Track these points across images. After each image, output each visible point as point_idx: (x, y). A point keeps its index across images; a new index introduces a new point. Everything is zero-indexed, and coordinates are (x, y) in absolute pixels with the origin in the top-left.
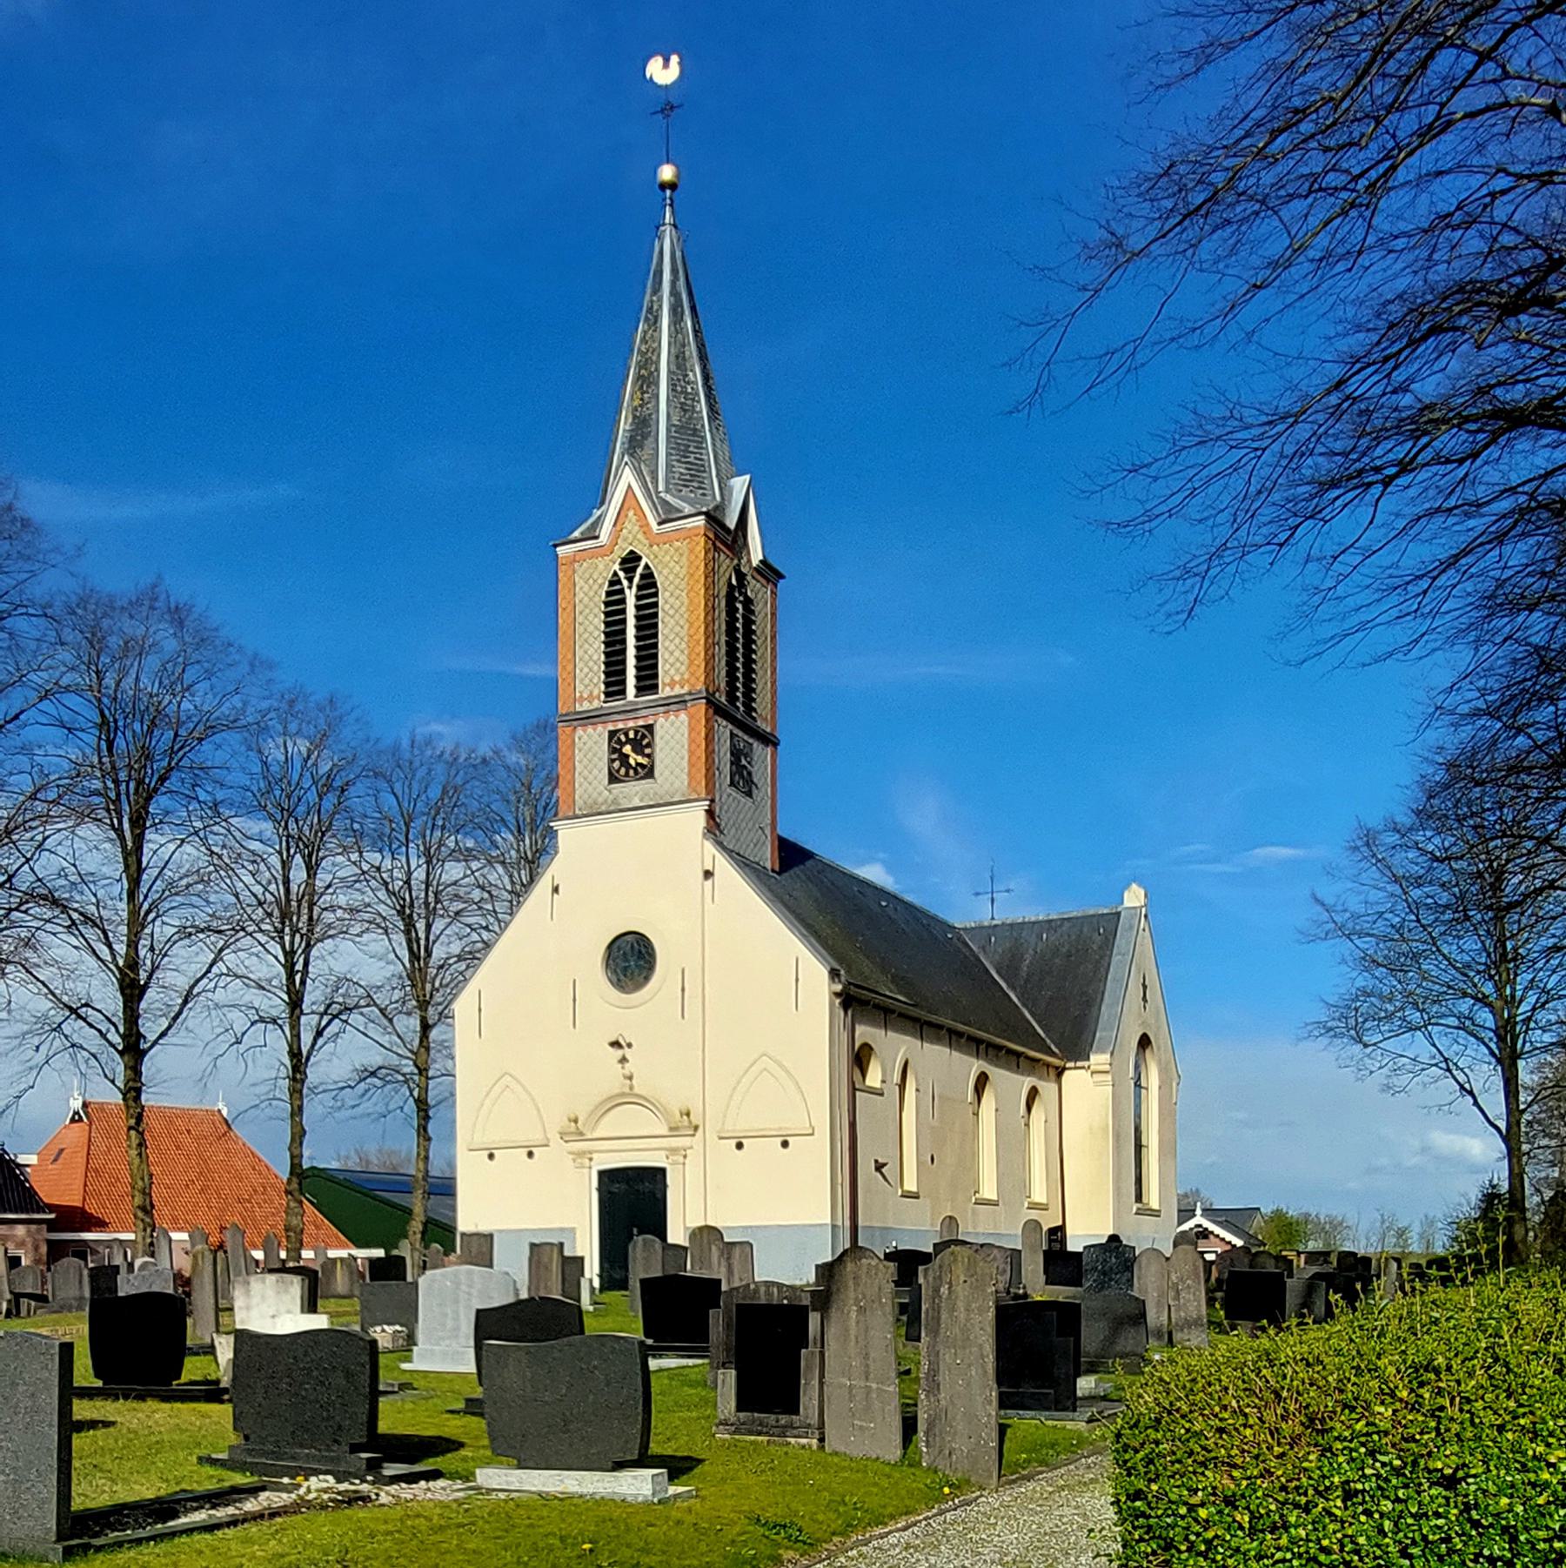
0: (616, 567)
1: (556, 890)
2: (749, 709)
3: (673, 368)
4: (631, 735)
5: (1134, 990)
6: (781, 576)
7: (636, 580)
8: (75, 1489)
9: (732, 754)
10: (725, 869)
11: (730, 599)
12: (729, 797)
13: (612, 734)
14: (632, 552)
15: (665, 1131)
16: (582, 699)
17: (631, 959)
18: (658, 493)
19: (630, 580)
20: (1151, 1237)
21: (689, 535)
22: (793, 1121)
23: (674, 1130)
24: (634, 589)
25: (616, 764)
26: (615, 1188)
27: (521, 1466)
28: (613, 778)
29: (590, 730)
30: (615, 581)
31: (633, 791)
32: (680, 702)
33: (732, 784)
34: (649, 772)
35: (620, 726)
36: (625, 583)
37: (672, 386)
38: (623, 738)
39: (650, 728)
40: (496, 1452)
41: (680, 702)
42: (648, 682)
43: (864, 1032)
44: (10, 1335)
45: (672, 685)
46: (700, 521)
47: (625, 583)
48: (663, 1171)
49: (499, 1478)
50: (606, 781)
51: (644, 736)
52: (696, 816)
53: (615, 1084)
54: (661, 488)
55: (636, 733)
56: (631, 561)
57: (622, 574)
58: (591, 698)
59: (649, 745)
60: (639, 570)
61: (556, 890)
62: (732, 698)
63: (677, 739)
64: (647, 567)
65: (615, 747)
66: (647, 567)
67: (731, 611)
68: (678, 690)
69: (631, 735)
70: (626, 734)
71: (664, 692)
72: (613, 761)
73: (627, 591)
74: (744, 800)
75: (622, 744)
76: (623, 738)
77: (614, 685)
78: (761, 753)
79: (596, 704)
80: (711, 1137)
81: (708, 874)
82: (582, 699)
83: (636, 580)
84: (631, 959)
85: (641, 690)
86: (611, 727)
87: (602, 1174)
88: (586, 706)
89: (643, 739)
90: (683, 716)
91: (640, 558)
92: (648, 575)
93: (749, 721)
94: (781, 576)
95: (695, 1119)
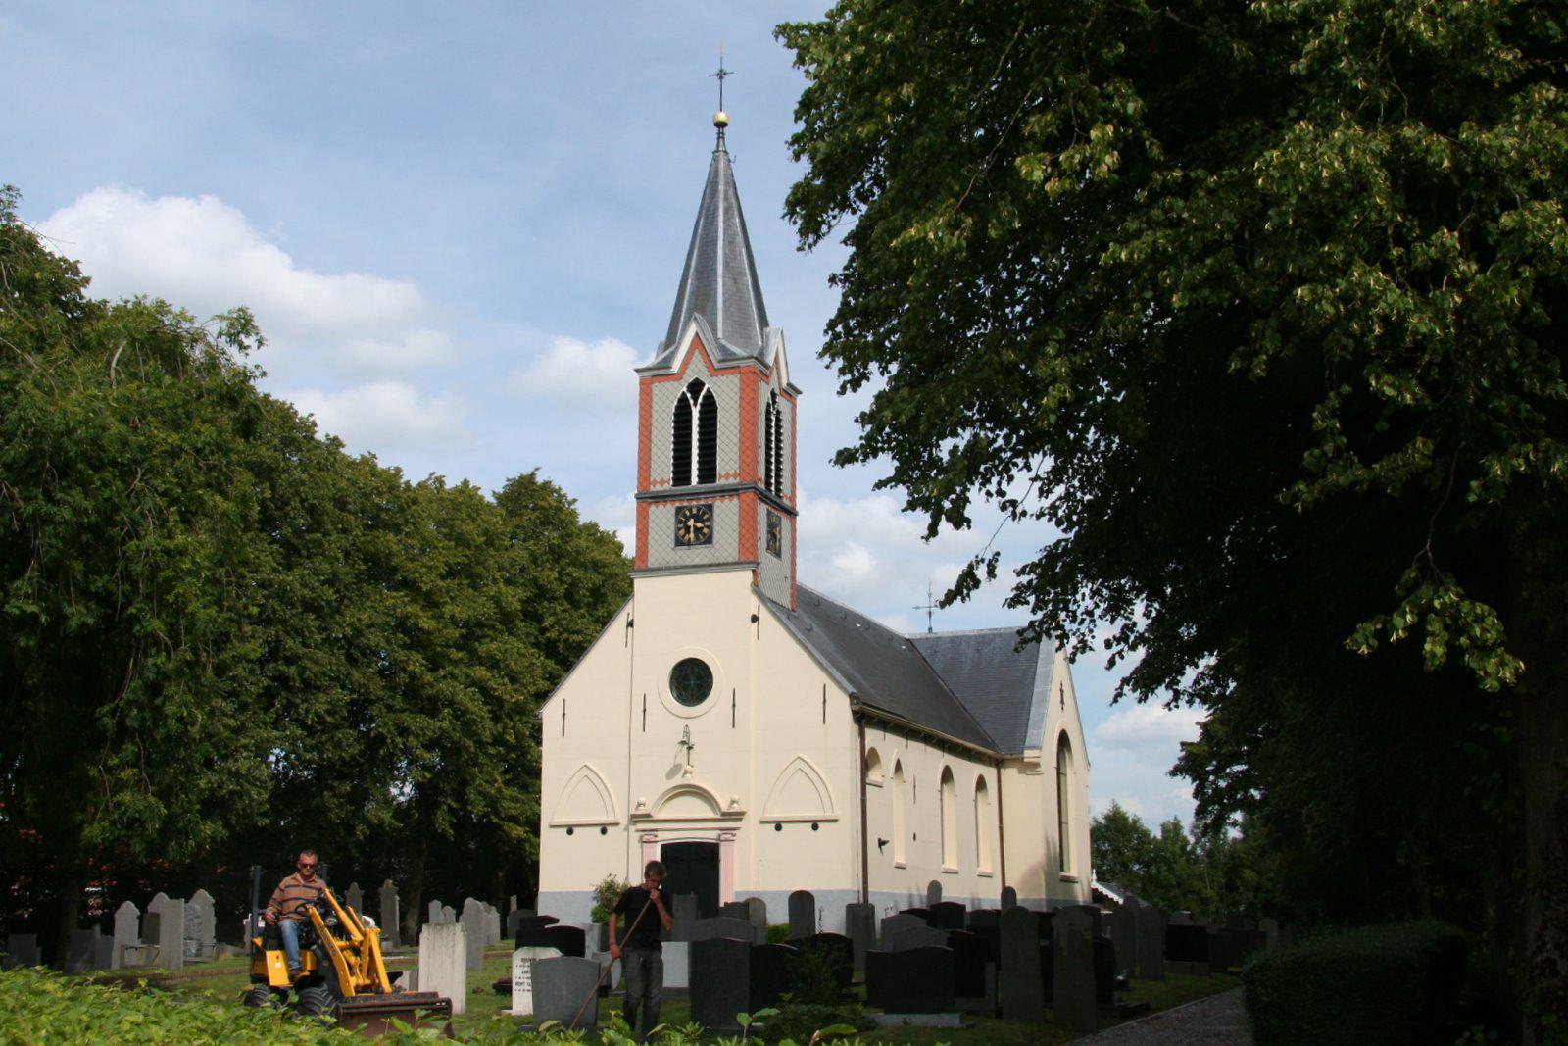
0: (685, 389)
1: (630, 624)
2: (778, 490)
3: (730, 283)
4: (694, 511)
5: (1055, 696)
6: (799, 392)
7: (700, 400)
8: (730, 559)
9: (769, 526)
10: (765, 615)
13: (679, 510)
14: (697, 379)
17: (692, 681)
18: (717, 339)
19: (695, 400)
24: (698, 407)
25: (682, 532)
28: (679, 542)
29: (661, 506)
30: (683, 400)
31: (698, 554)
33: (768, 548)
35: (686, 504)
36: (692, 402)
37: (727, 264)
38: (688, 513)
39: (710, 508)
42: (708, 472)
43: (874, 737)
44: (1414, 6)
47: (692, 402)
50: (673, 544)
51: (704, 513)
54: (720, 335)
55: (698, 510)
56: (696, 387)
57: (689, 395)
59: (708, 519)
60: (703, 393)
61: (630, 624)
62: (768, 484)
64: (708, 390)
65: (681, 517)
66: (708, 390)
68: (732, 481)
69: (694, 511)
70: (690, 510)
71: (720, 482)
72: (680, 529)
73: (693, 408)
74: (775, 560)
75: (688, 519)
76: (688, 513)
77: (681, 474)
78: (785, 522)
82: (655, 483)
83: (700, 400)
84: (692, 681)
85: (702, 479)
86: (678, 504)
88: (658, 488)
89: (705, 514)
90: (735, 501)
91: (703, 385)
92: (709, 397)
93: (778, 501)
94: (799, 392)
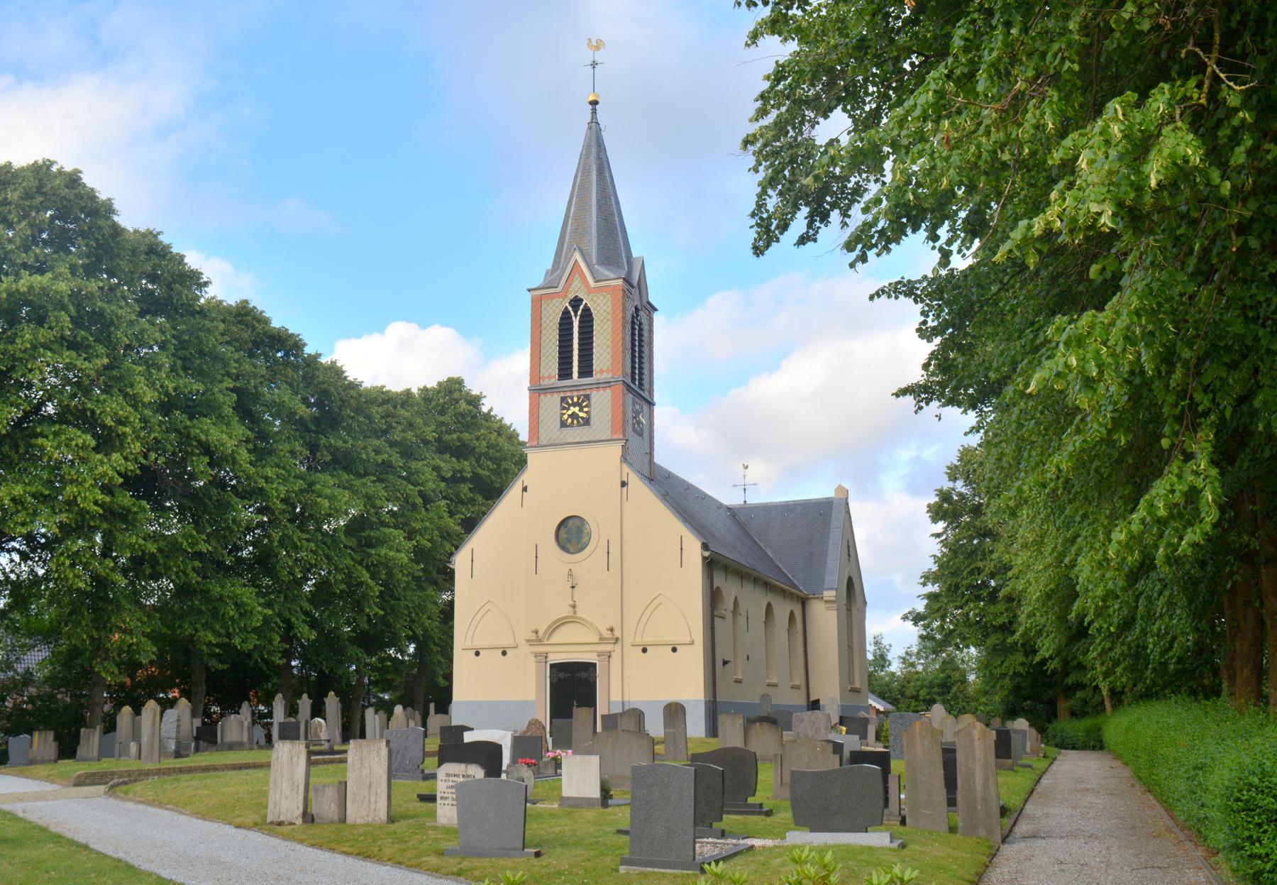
1: (525, 489)
11: (633, 323)
12: (634, 440)
15: (596, 640)
16: (544, 378)
20: (1050, 726)
21: (613, 289)
22: (680, 636)
23: (602, 640)
26: (562, 675)
27: (812, 831)
29: (549, 396)
30: (566, 312)
32: (607, 384)
34: (587, 422)
40: (797, 824)
41: (607, 384)
42: (586, 370)
45: (602, 372)
46: (620, 282)
48: (594, 665)
49: (801, 838)
52: (616, 450)
53: (566, 611)
56: (576, 302)
58: (549, 377)
61: (525, 489)
62: (633, 380)
63: (603, 404)
67: (633, 329)
71: (597, 377)
77: (565, 372)
79: (553, 381)
80: (627, 648)
81: (623, 484)
82: (544, 378)
84: (571, 534)
85: (581, 375)
87: (552, 666)
90: (608, 391)
92: (587, 309)
95: (617, 633)
